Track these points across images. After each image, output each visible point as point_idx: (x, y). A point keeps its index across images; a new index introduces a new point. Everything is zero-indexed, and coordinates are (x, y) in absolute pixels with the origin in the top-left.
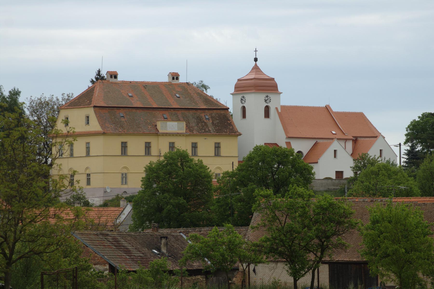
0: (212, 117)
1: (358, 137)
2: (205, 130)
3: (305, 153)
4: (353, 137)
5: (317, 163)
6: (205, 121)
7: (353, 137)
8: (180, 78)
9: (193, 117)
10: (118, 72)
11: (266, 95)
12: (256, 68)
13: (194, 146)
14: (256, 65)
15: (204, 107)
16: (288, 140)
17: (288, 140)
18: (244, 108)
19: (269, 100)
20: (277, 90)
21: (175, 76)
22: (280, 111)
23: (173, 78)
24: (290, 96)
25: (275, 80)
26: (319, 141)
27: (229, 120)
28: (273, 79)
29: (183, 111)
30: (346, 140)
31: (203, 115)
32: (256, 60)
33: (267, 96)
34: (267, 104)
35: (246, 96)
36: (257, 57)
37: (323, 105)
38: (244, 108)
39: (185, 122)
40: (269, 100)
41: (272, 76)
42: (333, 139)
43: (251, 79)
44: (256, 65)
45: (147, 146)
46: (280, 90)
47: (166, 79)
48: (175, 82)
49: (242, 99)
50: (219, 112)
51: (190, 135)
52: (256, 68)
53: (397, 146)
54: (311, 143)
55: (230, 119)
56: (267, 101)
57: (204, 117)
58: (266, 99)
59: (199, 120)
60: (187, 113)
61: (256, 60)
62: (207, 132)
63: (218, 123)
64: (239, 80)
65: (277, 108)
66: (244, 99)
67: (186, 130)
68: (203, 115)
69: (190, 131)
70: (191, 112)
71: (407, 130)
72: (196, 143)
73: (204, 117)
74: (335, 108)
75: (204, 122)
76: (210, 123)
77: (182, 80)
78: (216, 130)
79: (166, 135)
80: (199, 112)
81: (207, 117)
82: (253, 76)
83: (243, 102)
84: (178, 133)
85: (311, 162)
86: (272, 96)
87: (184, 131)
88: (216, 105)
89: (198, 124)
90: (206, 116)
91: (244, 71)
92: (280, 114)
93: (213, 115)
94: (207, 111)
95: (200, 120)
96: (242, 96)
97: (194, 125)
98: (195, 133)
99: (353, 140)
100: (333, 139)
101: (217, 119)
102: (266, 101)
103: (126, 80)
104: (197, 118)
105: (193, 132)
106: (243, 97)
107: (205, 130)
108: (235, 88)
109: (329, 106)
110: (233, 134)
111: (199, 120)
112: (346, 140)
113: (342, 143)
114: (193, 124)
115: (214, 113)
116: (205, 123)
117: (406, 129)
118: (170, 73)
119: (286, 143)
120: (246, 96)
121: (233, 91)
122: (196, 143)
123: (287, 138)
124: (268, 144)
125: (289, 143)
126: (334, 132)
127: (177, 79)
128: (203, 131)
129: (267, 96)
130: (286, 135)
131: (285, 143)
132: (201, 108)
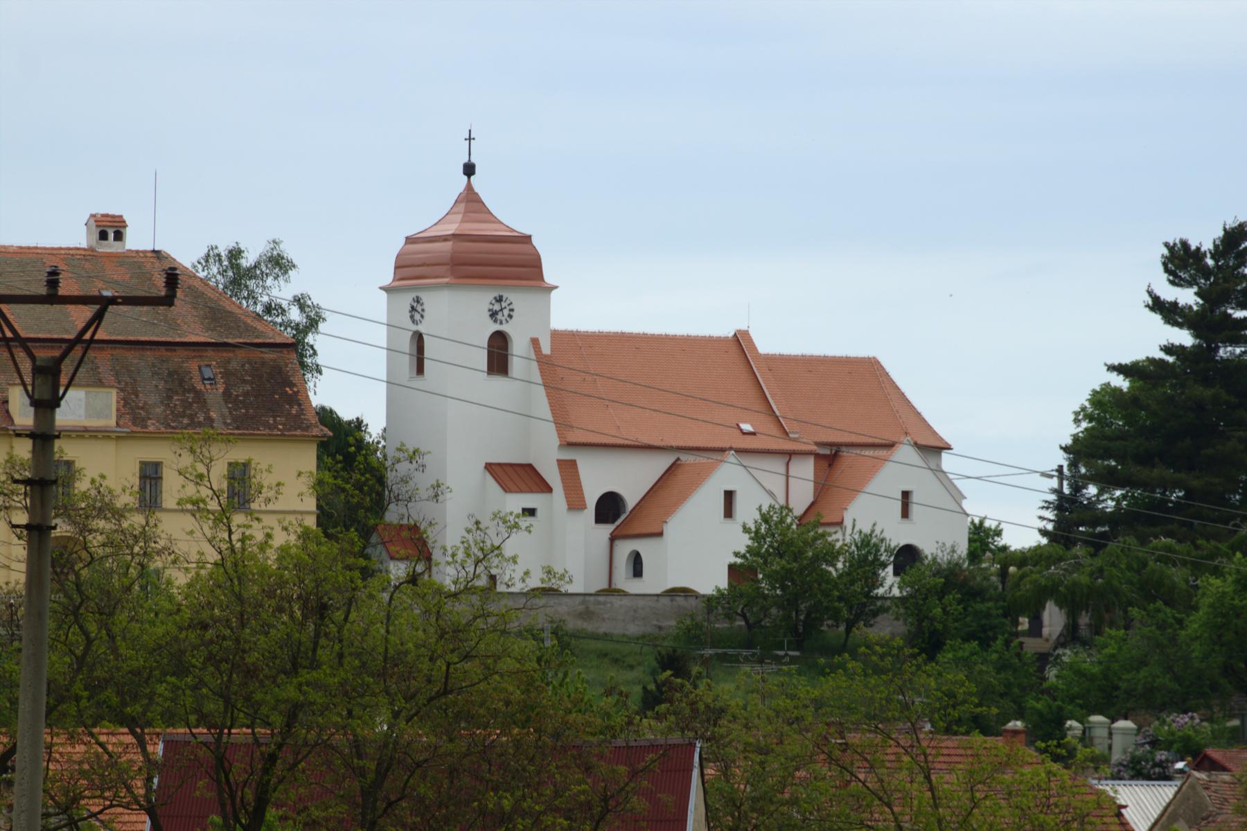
0: (227, 374)
1: (839, 445)
2: (192, 417)
3: (631, 502)
4: (817, 444)
5: (660, 534)
6: (199, 386)
7: (817, 444)
8: (129, 234)
9: (154, 373)
10: (125, 218)
11: (496, 294)
12: (470, 201)
13: (151, 475)
14: (469, 187)
15: (202, 339)
16: (568, 455)
17: (568, 455)
18: (419, 339)
19: (506, 312)
20: (539, 276)
21: (110, 228)
22: (546, 349)
23: (103, 236)
24: (586, 297)
25: (535, 241)
26: (686, 458)
27: (292, 385)
28: (527, 239)
29: (119, 352)
30: (790, 455)
31: (193, 366)
32: (469, 170)
33: (499, 300)
34: (497, 327)
35: (426, 297)
36: (473, 160)
37: (727, 331)
38: (419, 339)
39: (114, 392)
40: (506, 312)
41: (522, 228)
42: (722, 450)
43: (445, 239)
44: (469, 187)
45: (149, 472)
46: (549, 276)
47: (77, 237)
48: (111, 246)
49: (412, 307)
50: (257, 354)
51: (131, 436)
52: (470, 201)
53: (1051, 477)
54: (656, 466)
55: (295, 380)
56: (499, 317)
57: (195, 373)
58: (497, 307)
59: (178, 382)
60: (132, 357)
61: (469, 170)
62: (200, 424)
63: (246, 394)
64: (410, 240)
65: (535, 342)
66: (419, 308)
67: (119, 417)
68: (193, 366)
69: (137, 420)
70: (150, 355)
71: (1077, 421)
72: (157, 466)
73: (195, 373)
74: (766, 344)
75: (193, 389)
76: (215, 394)
77: (135, 240)
78: (235, 419)
79: (82, 437)
80: (178, 357)
81: (208, 373)
82: (451, 229)
83: (417, 317)
84: (86, 430)
85: (644, 531)
86: (519, 300)
87: (112, 422)
88: (249, 329)
89: (170, 398)
90: (212, 365)
91: (429, 209)
92: (544, 362)
93: (234, 365)
94: (210, 353)
95: (181, 382)
96: (414, 295)
97: (153, 399)
98: (151, 429)
99: (817, 456)
100: (722, 450)
101: (244, 382)
102: (493, 315)
103: (48, 246)
104: (170, 374)
105: (146, 427)
106: (418, 300)
107: (192, 417)
108: (396, 268)
109: (745, 334)
110: (298, 432)
111: (178, 382)
112: (790, 455)
113: (777, 465)
114: (150, 396)
115: (236, 360)
116: (198, 394)
117: (1073, 417)
118: (93, 216)
119: (562, 464)
120: (426, 297)
121: (388, 277)
122: (157, 466)
123: (561, 446)
124: (499, 465)
125: (573, 464)
126: (747, 427)
127: (119, 236)
128: (186, 421)
129: (499, 300)
130: (560, 435)
131: (555, 464)
132: (186, 340)
